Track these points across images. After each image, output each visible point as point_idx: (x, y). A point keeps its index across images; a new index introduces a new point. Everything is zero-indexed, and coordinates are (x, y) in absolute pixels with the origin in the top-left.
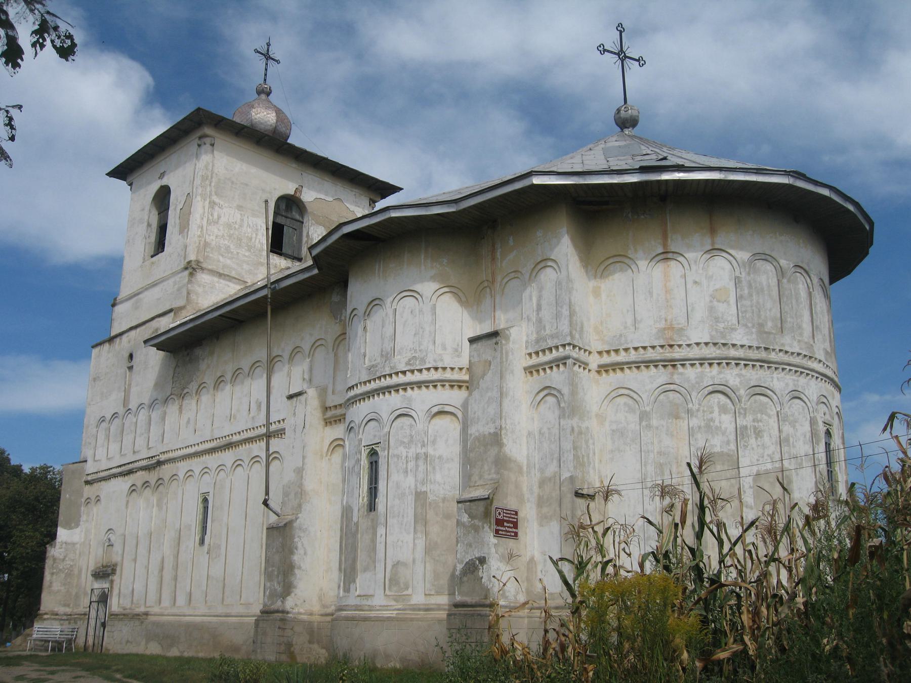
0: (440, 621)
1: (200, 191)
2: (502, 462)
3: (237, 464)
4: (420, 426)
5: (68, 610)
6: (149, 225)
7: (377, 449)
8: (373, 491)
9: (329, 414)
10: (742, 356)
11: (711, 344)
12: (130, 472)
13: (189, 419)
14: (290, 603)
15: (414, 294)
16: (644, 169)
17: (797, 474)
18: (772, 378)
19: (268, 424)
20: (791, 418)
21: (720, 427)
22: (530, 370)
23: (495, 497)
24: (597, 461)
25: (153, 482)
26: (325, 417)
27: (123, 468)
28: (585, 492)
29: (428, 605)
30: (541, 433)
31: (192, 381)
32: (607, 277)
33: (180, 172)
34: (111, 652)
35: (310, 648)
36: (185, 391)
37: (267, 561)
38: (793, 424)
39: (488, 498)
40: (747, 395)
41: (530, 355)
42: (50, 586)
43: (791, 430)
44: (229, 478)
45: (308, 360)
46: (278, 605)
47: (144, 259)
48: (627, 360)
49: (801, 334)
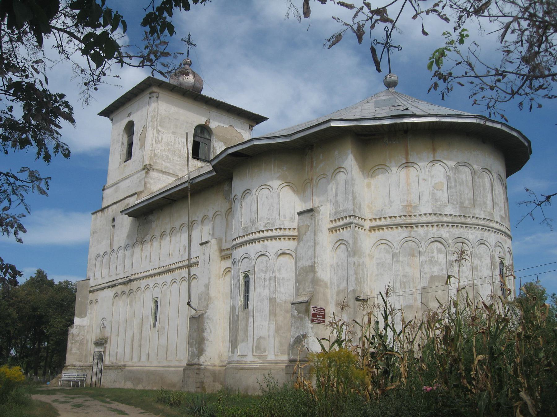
0: (282, 369)
1: (151, 124)
2: (316, 282)
3: (174, 282)
4: (272, 261)
5: (81, 364)
6: (123, 144)
7: (248, 274)
8: (247, 298)
9: (223, 253)
10: (451, 221)
11: (433, 215)
12: (114, 286)
13: (147, 256)
14: (202, 360)
15: (268, 187)
16: (393, 117)
17: (482, 287)
18: (468, 233)
19: (189, 260)
20: (479, 255)
21: (438, 261)
22: (332, 230)
23: (311, 301)
24: (369, 281)
25: (127, 291)
26: (221, 255)
27: (110, 283)
28: (361, 298)
29: (276, 360)
30: (338, 265)
31: (148, 234)
32: (375, 177)
33: (139, 113)
34: (105, 387)
35: (214, 385)
36: (144, 240)
37: (190, 336)
38: (480, 259)
39: (308, 302)
40: (453, 243)
41: (332, 221)
42: (71, 350)
43: (479, 262)
44: (169, 289)
45: (212, 223)
46: (196, 361)
47: (120, 163)
48: (385, 224)
49: (486, 207)
